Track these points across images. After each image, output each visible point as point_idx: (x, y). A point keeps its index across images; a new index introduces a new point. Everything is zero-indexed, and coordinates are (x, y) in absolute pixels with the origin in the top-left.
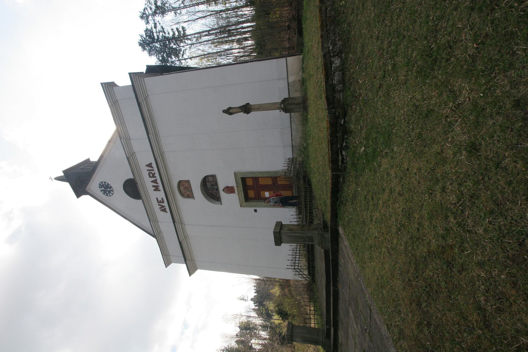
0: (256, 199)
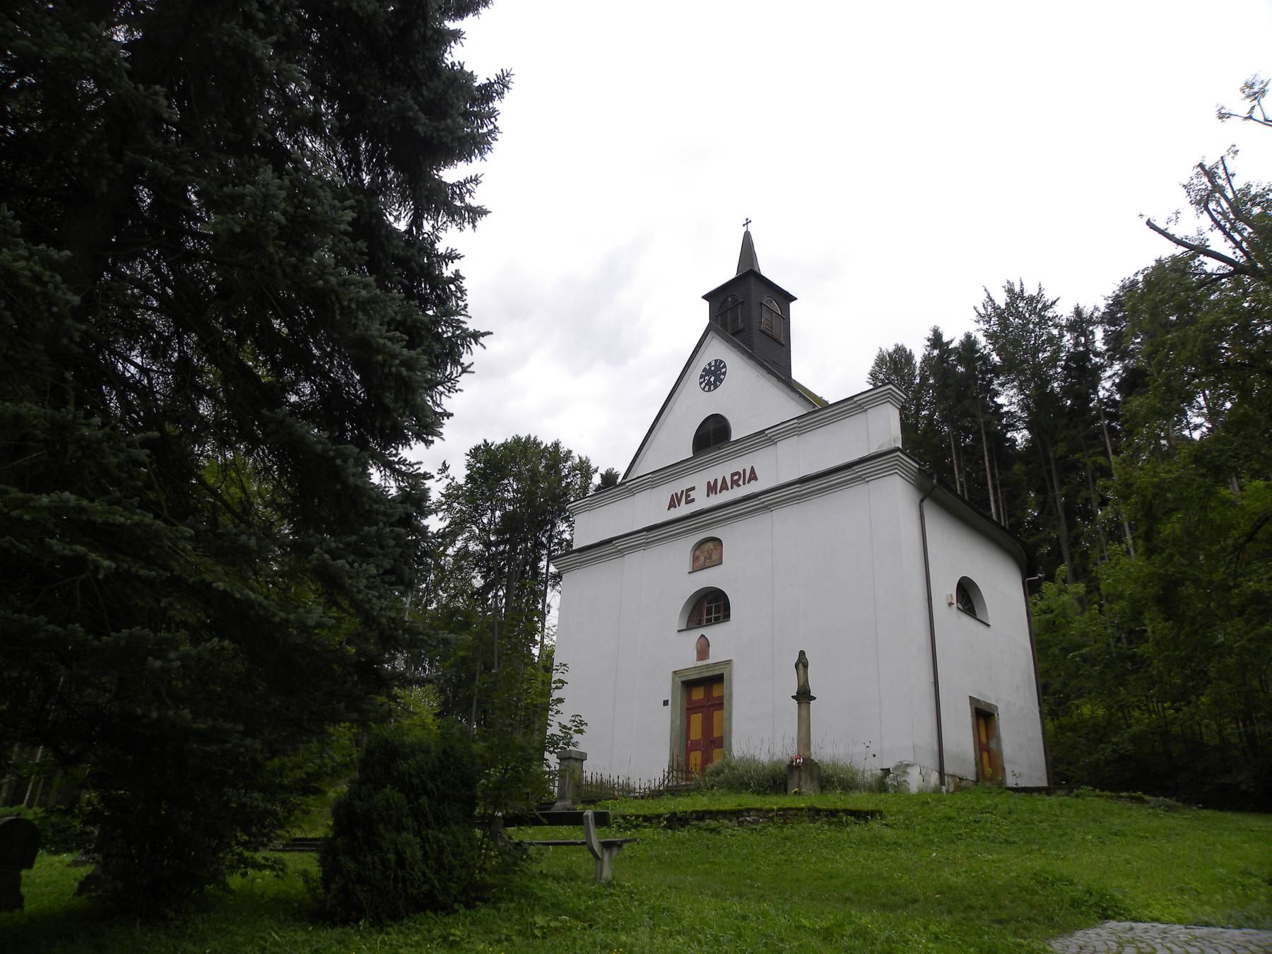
0: (688, 704)
